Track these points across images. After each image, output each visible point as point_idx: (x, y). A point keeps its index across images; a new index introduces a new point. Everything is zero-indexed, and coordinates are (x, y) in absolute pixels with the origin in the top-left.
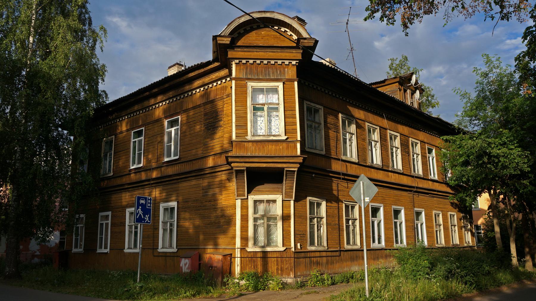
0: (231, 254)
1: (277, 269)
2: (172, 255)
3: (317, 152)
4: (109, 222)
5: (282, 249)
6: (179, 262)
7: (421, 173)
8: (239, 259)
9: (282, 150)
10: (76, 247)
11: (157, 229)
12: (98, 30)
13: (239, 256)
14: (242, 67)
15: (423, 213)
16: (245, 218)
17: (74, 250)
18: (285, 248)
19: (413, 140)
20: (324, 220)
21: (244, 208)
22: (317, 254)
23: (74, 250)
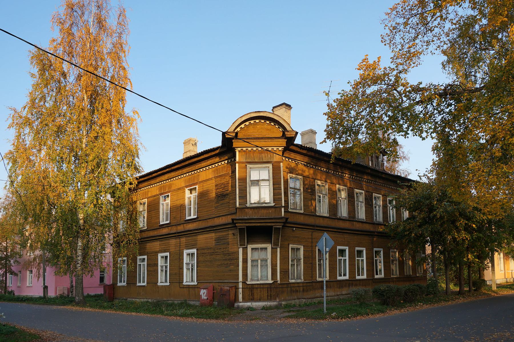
0: (236, 286)
1: (268, 296)
2: (194, 287)
3: (298, 211)
4: (146, 263)
5: (271, 282)
6: (199, 292)
7: (381, 220)
8: (241, 289)
9: (272, 214)
10: (121, 282)
11: (182, 268)
12: (131, 114)
13: (241, 287)
14: (243, 153)
15: (382, 252)
16: (245, 261)
17: (119, 284)
18: (273, 281)
19: (376, 195)
20: (302, 261)
21: (245, 254)
22: (296, 285)
23: (119, 284)
